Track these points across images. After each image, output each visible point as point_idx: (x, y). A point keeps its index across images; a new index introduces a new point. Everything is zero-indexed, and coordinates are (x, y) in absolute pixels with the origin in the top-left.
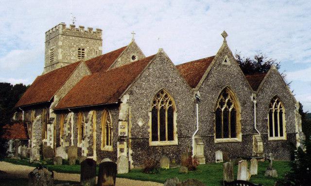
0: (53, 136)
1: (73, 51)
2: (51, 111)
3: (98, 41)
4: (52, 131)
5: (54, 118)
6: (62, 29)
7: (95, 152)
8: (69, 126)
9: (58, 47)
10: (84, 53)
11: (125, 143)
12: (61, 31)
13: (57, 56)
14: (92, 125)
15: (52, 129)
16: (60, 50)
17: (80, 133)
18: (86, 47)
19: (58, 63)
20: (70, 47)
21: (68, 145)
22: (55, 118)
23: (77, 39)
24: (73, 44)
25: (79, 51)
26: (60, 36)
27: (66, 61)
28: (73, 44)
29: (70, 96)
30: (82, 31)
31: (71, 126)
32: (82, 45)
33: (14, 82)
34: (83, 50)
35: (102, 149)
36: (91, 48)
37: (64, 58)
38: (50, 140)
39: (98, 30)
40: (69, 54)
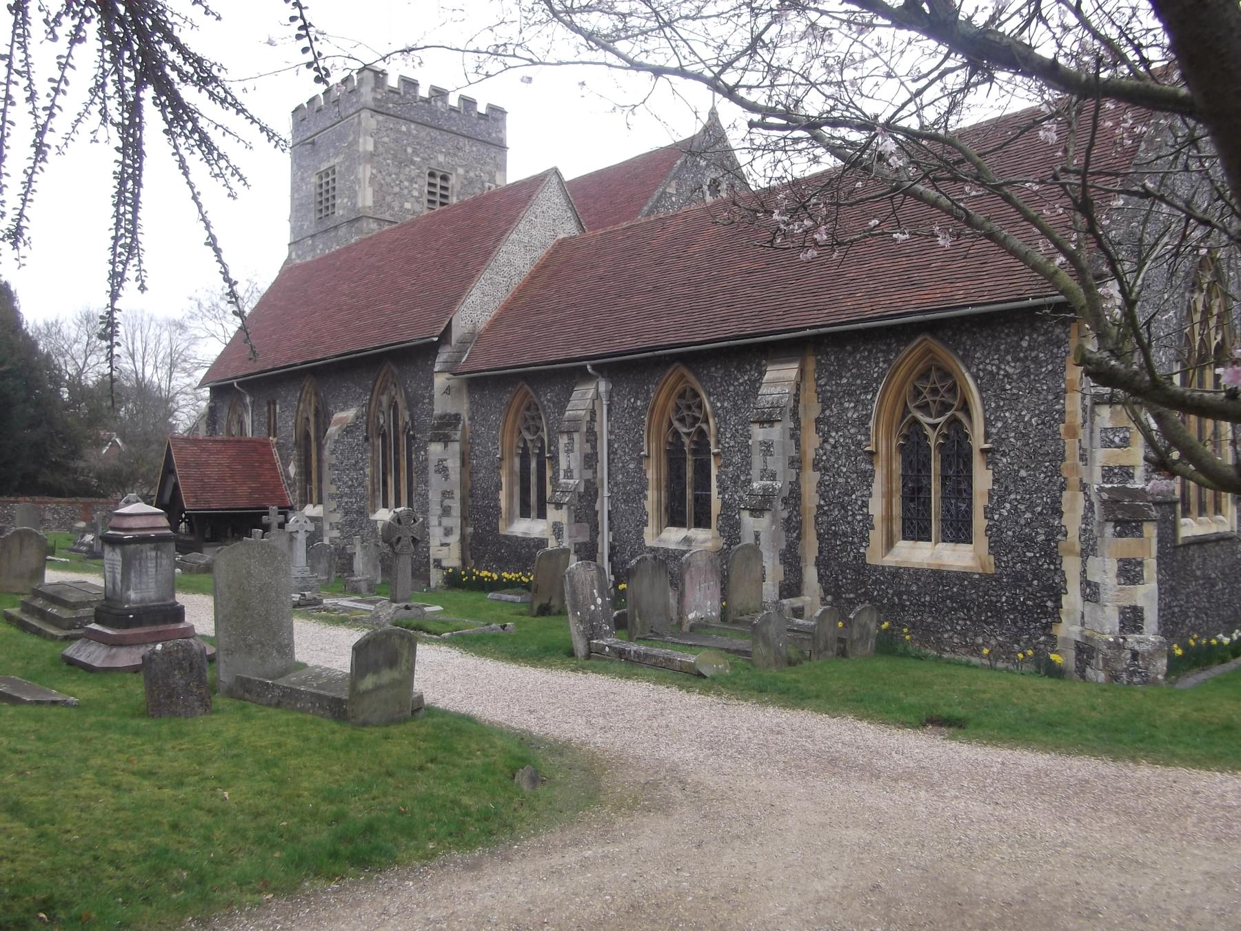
0: (457, 494)
1: (412, 180)
2: (440, 381)
3: (493, 149)
4: (455, 475)
5: (457, 417)
6: (374, 90)
7: (811, 574)
8: (588, 448)
9: (354, 159)
10: (445, 189)
11: (1150, 531)
12: (367, 95)
13: (353, 195)
14: (795, 435)
15: (453, 464)
16: (365, 172)
17: (659, 480)
18: (454, 168)
19: (358, 219)
20: (402, 163)
21: (587, 539)
22: (465, 416)
23: (424, 132)
24: (409, 150)
25: (432, 181)
26: (365, 114)
27: (387, 217)
28: (409, 150)
29: (521, 306)
30: (439, 104)
31: (594, 447)
32: (441, 158)
33: (144, 147)
34: (444, 178)
35: (876, 555)
36: (472, 174)
37: (379, 203)
38: (446, 511)
39: (492, 108)
40: (397, 189)
